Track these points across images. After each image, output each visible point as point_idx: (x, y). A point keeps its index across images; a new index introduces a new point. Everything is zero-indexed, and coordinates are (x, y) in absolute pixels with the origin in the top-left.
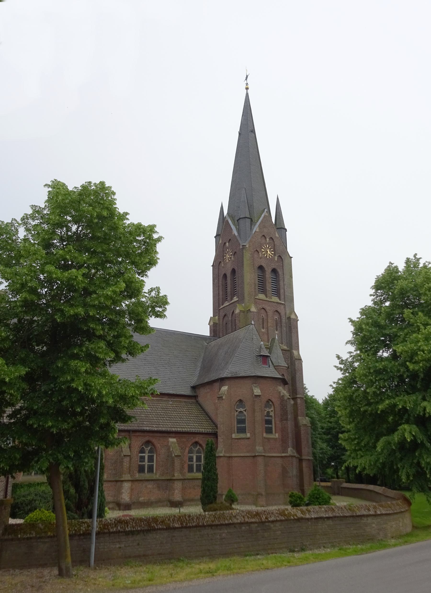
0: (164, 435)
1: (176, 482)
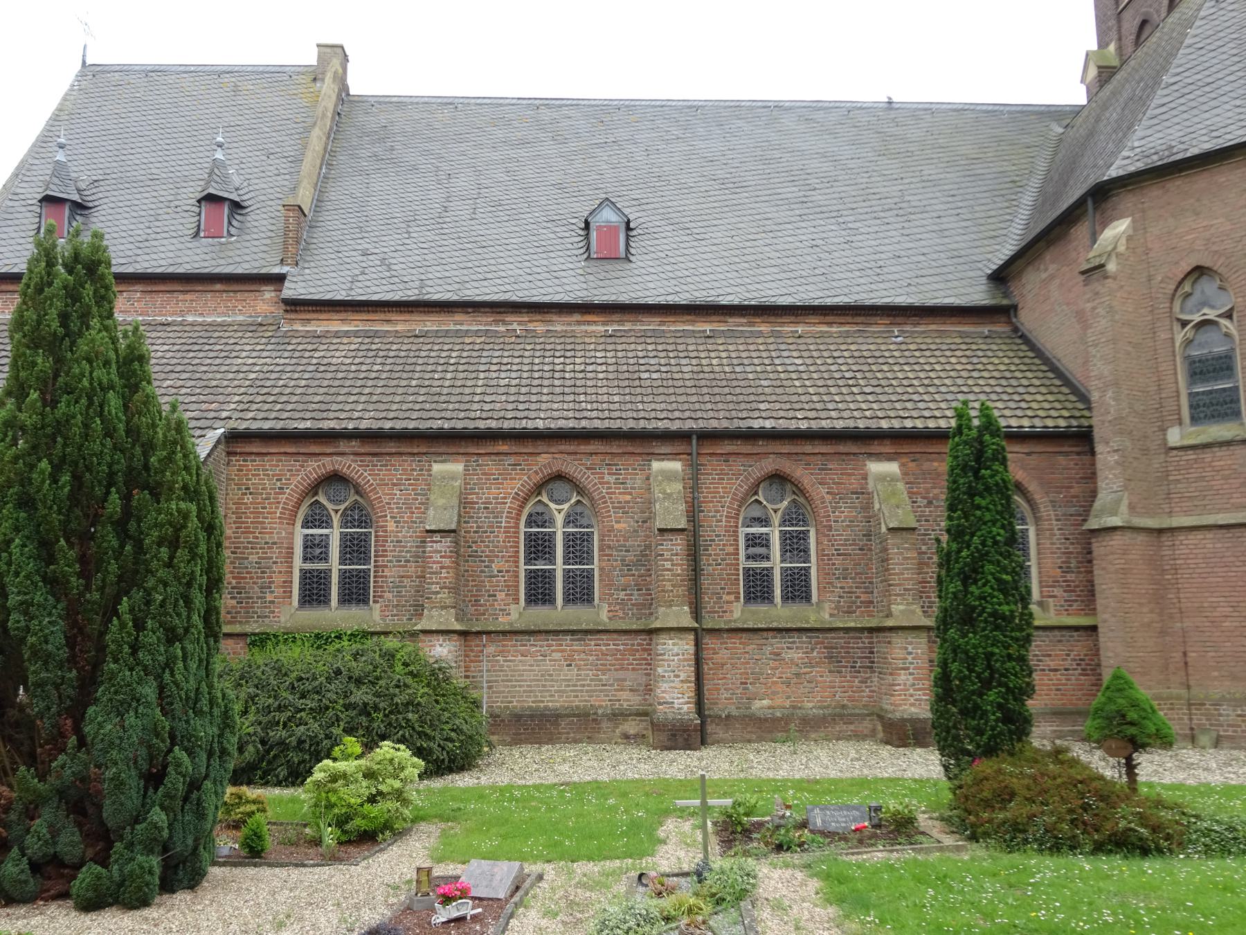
0: (842, 448)
1: (898, 640)
